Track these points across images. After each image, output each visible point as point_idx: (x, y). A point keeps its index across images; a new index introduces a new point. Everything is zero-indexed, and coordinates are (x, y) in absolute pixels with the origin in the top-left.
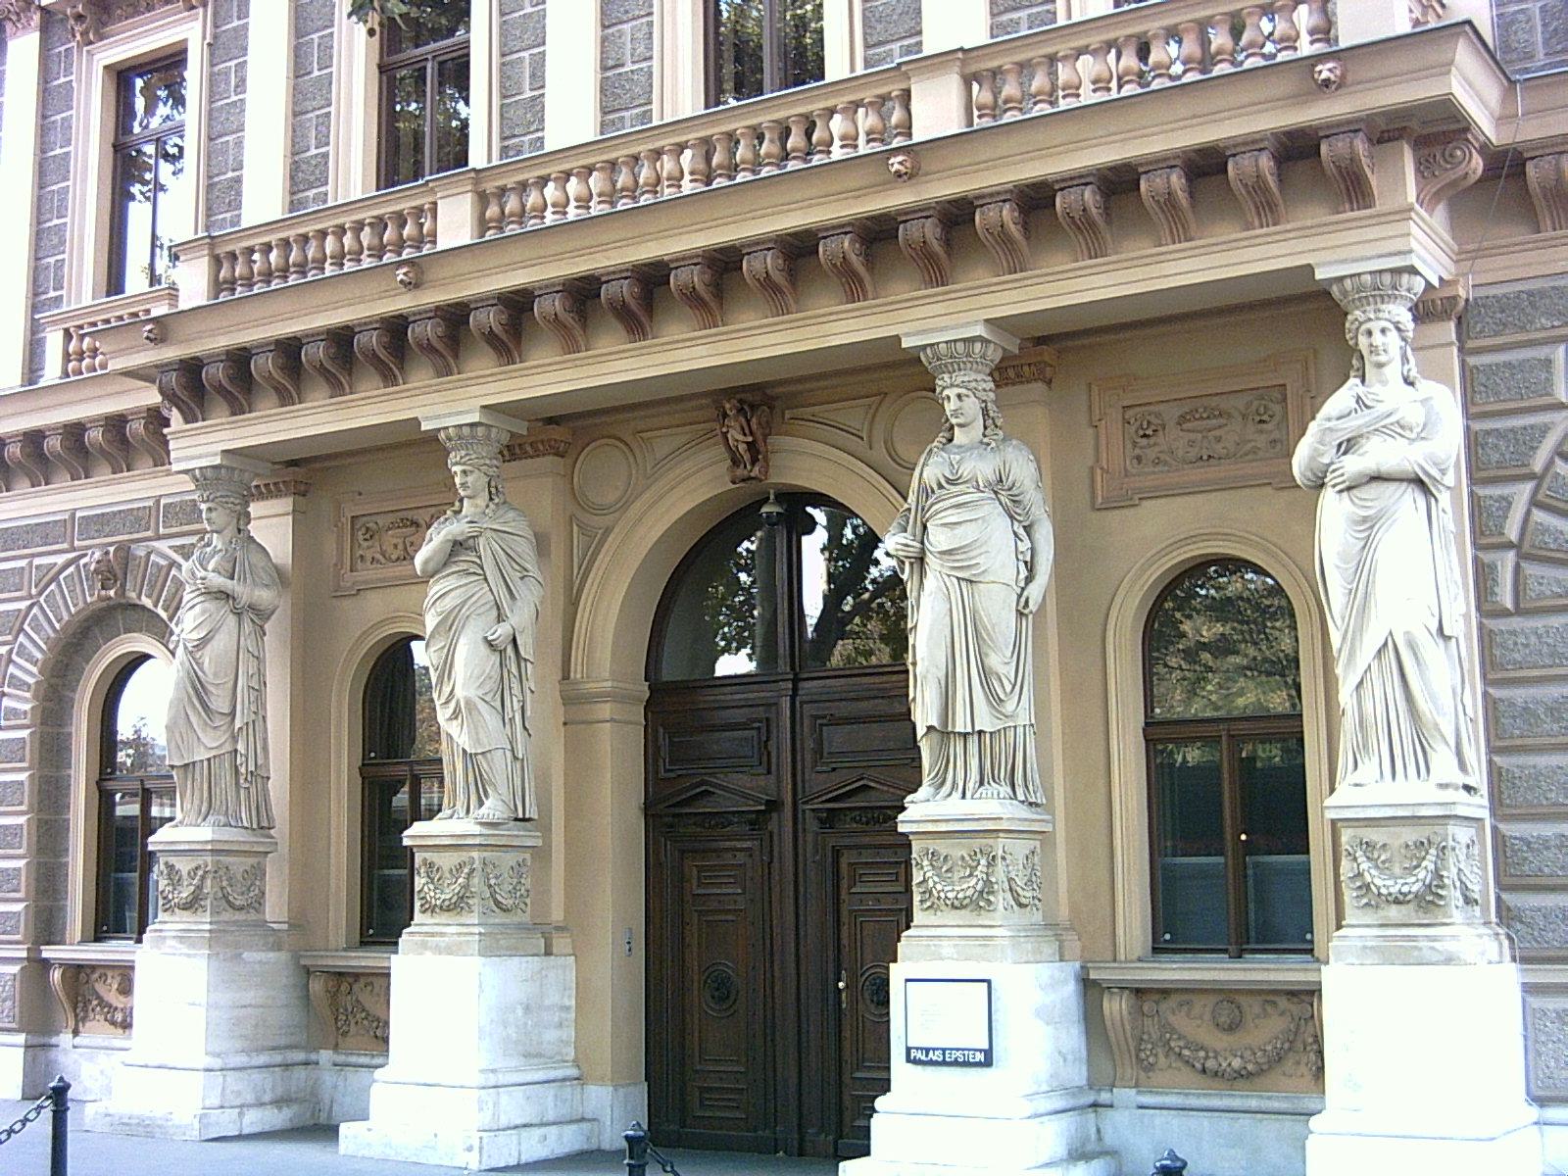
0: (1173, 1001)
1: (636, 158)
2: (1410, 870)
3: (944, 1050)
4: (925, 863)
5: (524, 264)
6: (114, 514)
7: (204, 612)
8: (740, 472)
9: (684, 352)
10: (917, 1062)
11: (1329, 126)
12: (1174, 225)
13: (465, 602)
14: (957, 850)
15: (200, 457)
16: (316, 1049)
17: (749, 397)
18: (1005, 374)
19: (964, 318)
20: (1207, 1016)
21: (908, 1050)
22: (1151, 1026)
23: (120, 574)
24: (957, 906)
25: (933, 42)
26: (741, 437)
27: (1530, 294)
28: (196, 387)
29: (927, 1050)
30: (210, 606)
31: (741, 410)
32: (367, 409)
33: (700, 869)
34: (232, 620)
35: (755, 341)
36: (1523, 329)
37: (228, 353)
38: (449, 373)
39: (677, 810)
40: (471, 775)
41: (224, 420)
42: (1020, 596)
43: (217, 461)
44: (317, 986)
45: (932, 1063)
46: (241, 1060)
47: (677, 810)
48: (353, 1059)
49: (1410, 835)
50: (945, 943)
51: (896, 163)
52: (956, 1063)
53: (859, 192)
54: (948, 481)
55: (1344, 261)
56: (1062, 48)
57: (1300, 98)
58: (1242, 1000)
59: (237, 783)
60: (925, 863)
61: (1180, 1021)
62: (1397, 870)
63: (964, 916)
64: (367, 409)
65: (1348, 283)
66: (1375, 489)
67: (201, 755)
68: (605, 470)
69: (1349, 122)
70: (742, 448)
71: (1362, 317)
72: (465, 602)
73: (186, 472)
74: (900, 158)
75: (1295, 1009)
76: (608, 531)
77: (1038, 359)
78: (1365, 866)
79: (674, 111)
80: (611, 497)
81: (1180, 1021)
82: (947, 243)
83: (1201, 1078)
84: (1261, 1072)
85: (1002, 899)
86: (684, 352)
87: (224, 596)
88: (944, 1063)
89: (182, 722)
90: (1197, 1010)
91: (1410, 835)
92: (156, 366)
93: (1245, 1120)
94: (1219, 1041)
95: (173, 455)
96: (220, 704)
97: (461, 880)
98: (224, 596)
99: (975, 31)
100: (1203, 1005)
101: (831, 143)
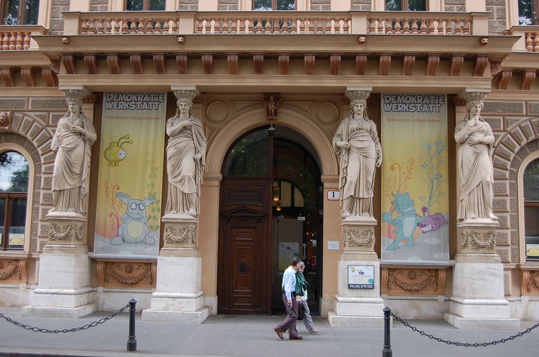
0: (397, 272)
1: (274, 20)
2: (486, 240)
3: (360, 285)
4: (351, 233)
5: (226, 45)
6: (8, 101)
7: (73, 139)
8: (270, 117)
9: (251, 81)
10: (352, 288)
11: (480, 54)
12: (408, 71)
13: (186, 146)
14: (361, 230)
15: (73, 86)
16: (97, 287)
17: (277, 96)
18: (196, 101)
19: (367, 85)
20: (406, 276)
21: (349, 285)
22: (109, 271)
23: (10, 121)
24: (60, 239)
25: (73, 8)
26: (274, 107)
27: (496, 103)
28: (76, 62)
29: (355, 285)
30: (75, 137)
31: (274, 100)
32: (329, 82)
33: (237, 232)
34: (82, 142)
35: (274, 81)
36: (494, 111)
37: (239, 53)
38: (72, 73)
39: (233, 215)
40: (185, 201)
41: (86, 75)
42: (376, 162)
43: (81, 88)
44: (100, 267)
45: (356, 288)
46: (80, 291)
47: (233, 215)
48: (113, 290)
49: (486, 231)
50: (358, 255)
51: (180, 39)
52: (364, 288)
53: (346, 45)
54: (359, 128)
55: (474, 88)
56: (294, 17)
57: (474, 46)
58: (416, 272)
59: (79, 198)
60: (351, 233)
61: (117, 270)
62: (482, 239)
63: (61, 242)
64: (329, 82)
65: (355, 92)
66: (478, 146)
67: (67, 187)
68: (218, 113)
69: (485, 54)
70: (273, 111)
71: (475, 103)
72: (186, 146)
73: (65, 91)
74: (65, 39)
75: (146, 268)
76: (220, 130)
77: (204, 99)
78: (476, 238)
79: (111, 9)
80: (220, 118)
81: (117, 270)
82: (142, 62)
83: (404, 292)
84: (136, 283)
85: (73, 238)
86: (251, 81)
87: (81, 134)
88: (360, 288)
89: (61, 175)
90: (121, 267)
91: (486, 231)
92: (62, 53)
93: (417, 302)
94: (409, 282)
95: (60, 84)
96: (77, 170)
97: (185, 233)
98: (81, 134)
99: (85, 8)
100: (405, 273)
101: (111, 29)
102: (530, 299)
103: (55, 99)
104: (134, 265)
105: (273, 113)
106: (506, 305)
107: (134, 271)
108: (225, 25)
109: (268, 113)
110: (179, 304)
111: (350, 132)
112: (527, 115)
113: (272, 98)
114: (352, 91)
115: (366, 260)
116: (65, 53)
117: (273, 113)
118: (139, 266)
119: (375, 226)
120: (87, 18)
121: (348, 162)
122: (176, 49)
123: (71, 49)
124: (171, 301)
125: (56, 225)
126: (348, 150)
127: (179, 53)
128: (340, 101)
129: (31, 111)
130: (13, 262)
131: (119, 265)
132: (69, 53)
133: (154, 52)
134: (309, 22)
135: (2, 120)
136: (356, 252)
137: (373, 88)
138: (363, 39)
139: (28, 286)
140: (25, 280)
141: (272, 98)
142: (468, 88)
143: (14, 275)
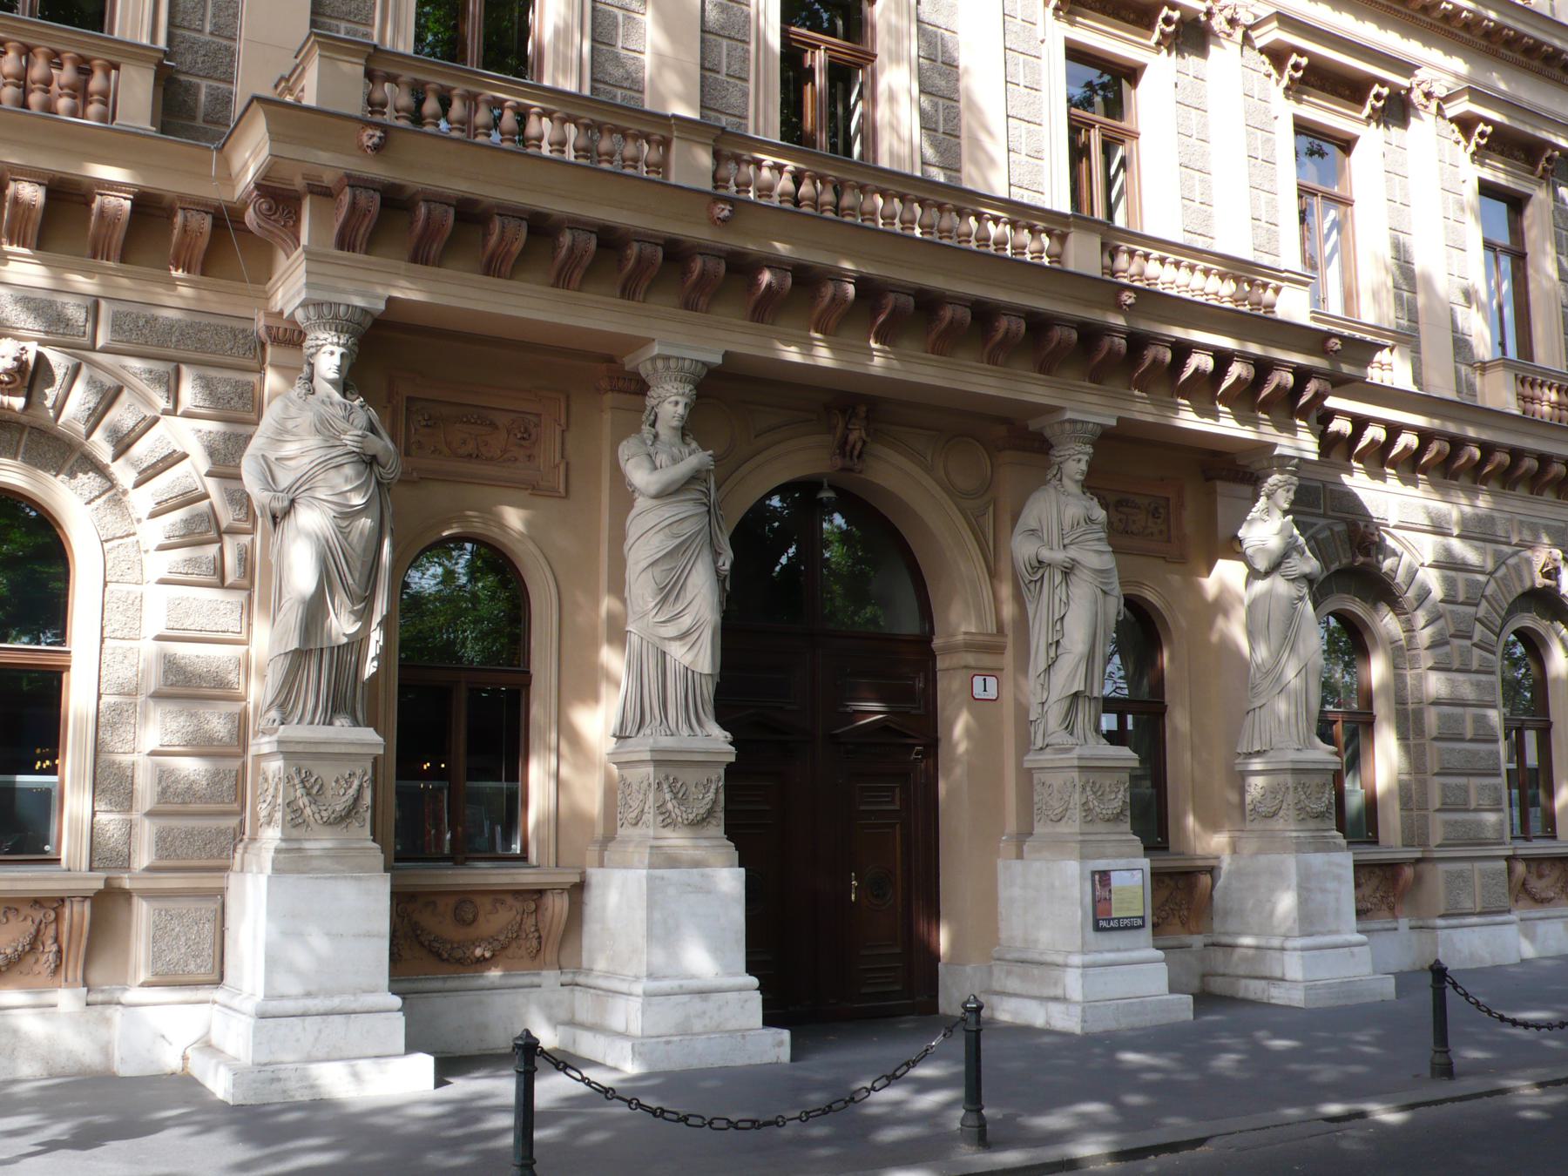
70: (859, 445)
102: (1413, 923)
103: (205, 320)
104: (478, 900)
105: (856, 453)
106: (1362, 944)
107: (481, 919)
108: (605, 144)
109: (843, 448)
110: (720, 1008)
111: (1067, 528)
112: (1325, 516)
113: (862, 410)
114: (1073, 422)
115: (1121, 856)
116: (359, 178)
117: (856, 453)
118: (496, 901)
119: (1133, 768)
120: (394, 70)
121: (1067, 604)
122: (699, 233)
123: (733, 241)
124: (697, 1004)
125: (309, 774)
126: (1068, 571)
127: (707, 247)
128: (1024, 441)
129: (104, 350)
130: (26, 910)
131: (434, 903)
132: (373, 181)
133: (699, 246)
134: (646, 147)
135: (6, 372)
136: (1099, 837)
137: (1120, 419)
138: (1335, 344)
139: (94, 997)
140: (74, 969)
141: (862, 410)
142: (1073, 410)
143: (31, 959)
